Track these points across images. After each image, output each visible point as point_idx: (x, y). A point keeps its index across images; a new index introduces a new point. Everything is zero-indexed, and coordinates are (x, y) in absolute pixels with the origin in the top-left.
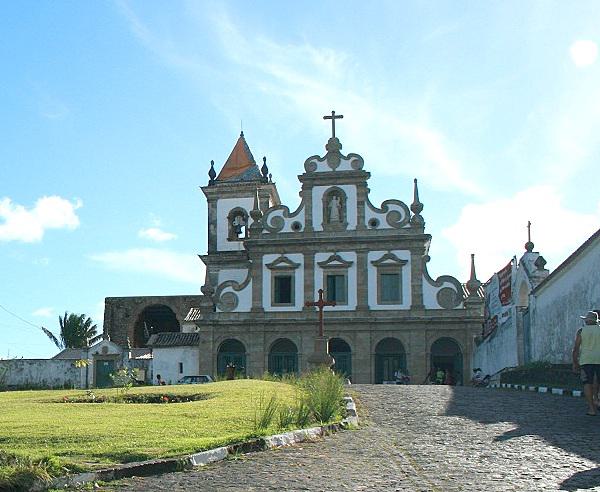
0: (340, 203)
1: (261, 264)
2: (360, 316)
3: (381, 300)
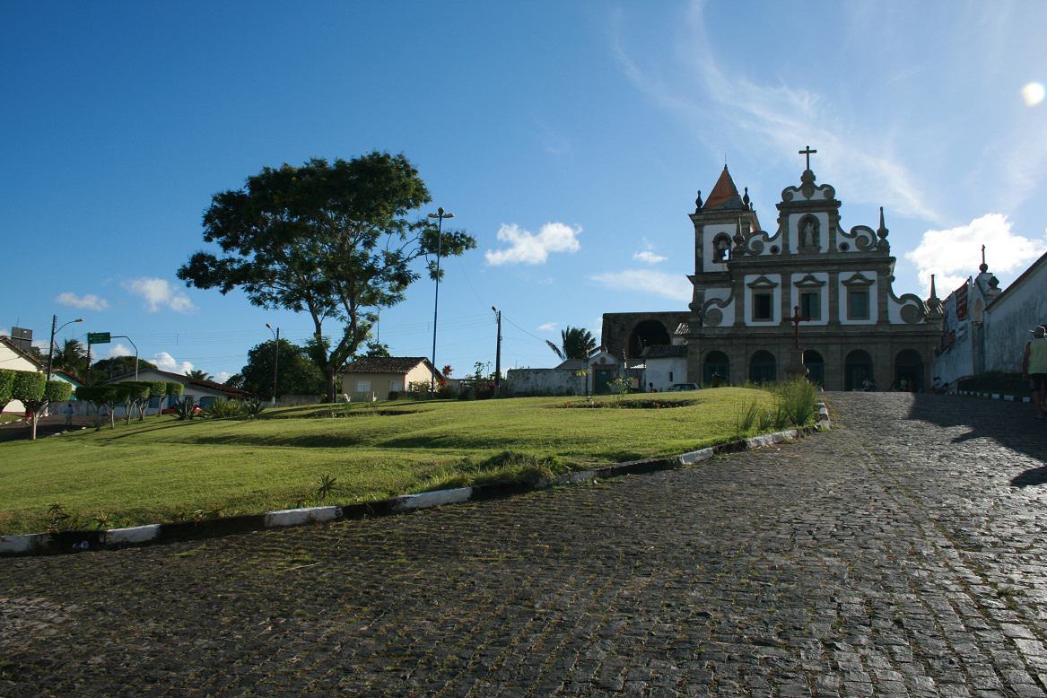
0: (814, 229)
3: (851, 316)
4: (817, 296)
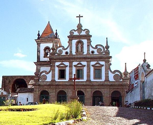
0: (82, 45)
1: (55, 65)
2: (88, 83)
3: (95, 78)
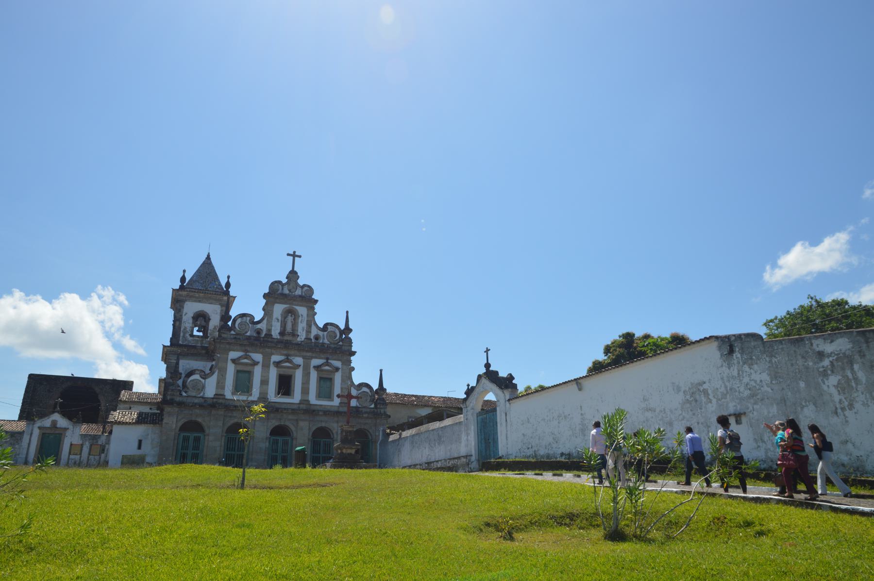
0: (294, 319)
2: (303, 406)
3: (319, 396)
4: (250, 373)
